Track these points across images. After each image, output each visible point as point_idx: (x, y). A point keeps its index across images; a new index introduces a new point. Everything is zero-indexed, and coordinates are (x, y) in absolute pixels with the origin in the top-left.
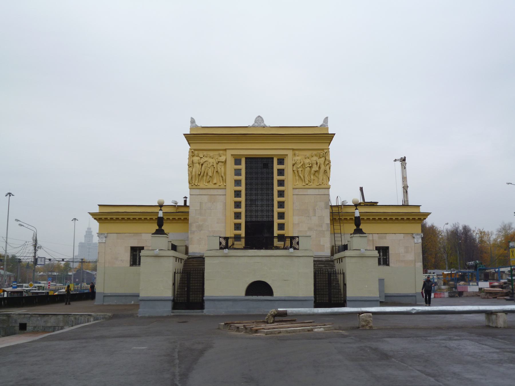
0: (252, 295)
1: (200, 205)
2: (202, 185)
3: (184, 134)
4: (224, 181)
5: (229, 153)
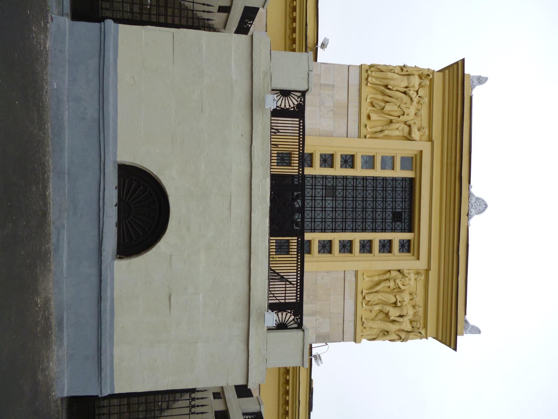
0: (120, 187)
1: (329, 85)
2: (367, 91)
3: (463, 60)
4: (375, 135)
5: (425, 147)
